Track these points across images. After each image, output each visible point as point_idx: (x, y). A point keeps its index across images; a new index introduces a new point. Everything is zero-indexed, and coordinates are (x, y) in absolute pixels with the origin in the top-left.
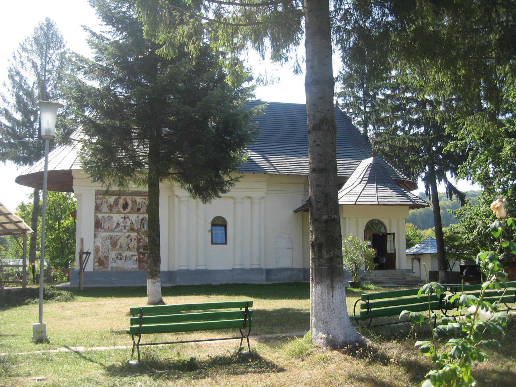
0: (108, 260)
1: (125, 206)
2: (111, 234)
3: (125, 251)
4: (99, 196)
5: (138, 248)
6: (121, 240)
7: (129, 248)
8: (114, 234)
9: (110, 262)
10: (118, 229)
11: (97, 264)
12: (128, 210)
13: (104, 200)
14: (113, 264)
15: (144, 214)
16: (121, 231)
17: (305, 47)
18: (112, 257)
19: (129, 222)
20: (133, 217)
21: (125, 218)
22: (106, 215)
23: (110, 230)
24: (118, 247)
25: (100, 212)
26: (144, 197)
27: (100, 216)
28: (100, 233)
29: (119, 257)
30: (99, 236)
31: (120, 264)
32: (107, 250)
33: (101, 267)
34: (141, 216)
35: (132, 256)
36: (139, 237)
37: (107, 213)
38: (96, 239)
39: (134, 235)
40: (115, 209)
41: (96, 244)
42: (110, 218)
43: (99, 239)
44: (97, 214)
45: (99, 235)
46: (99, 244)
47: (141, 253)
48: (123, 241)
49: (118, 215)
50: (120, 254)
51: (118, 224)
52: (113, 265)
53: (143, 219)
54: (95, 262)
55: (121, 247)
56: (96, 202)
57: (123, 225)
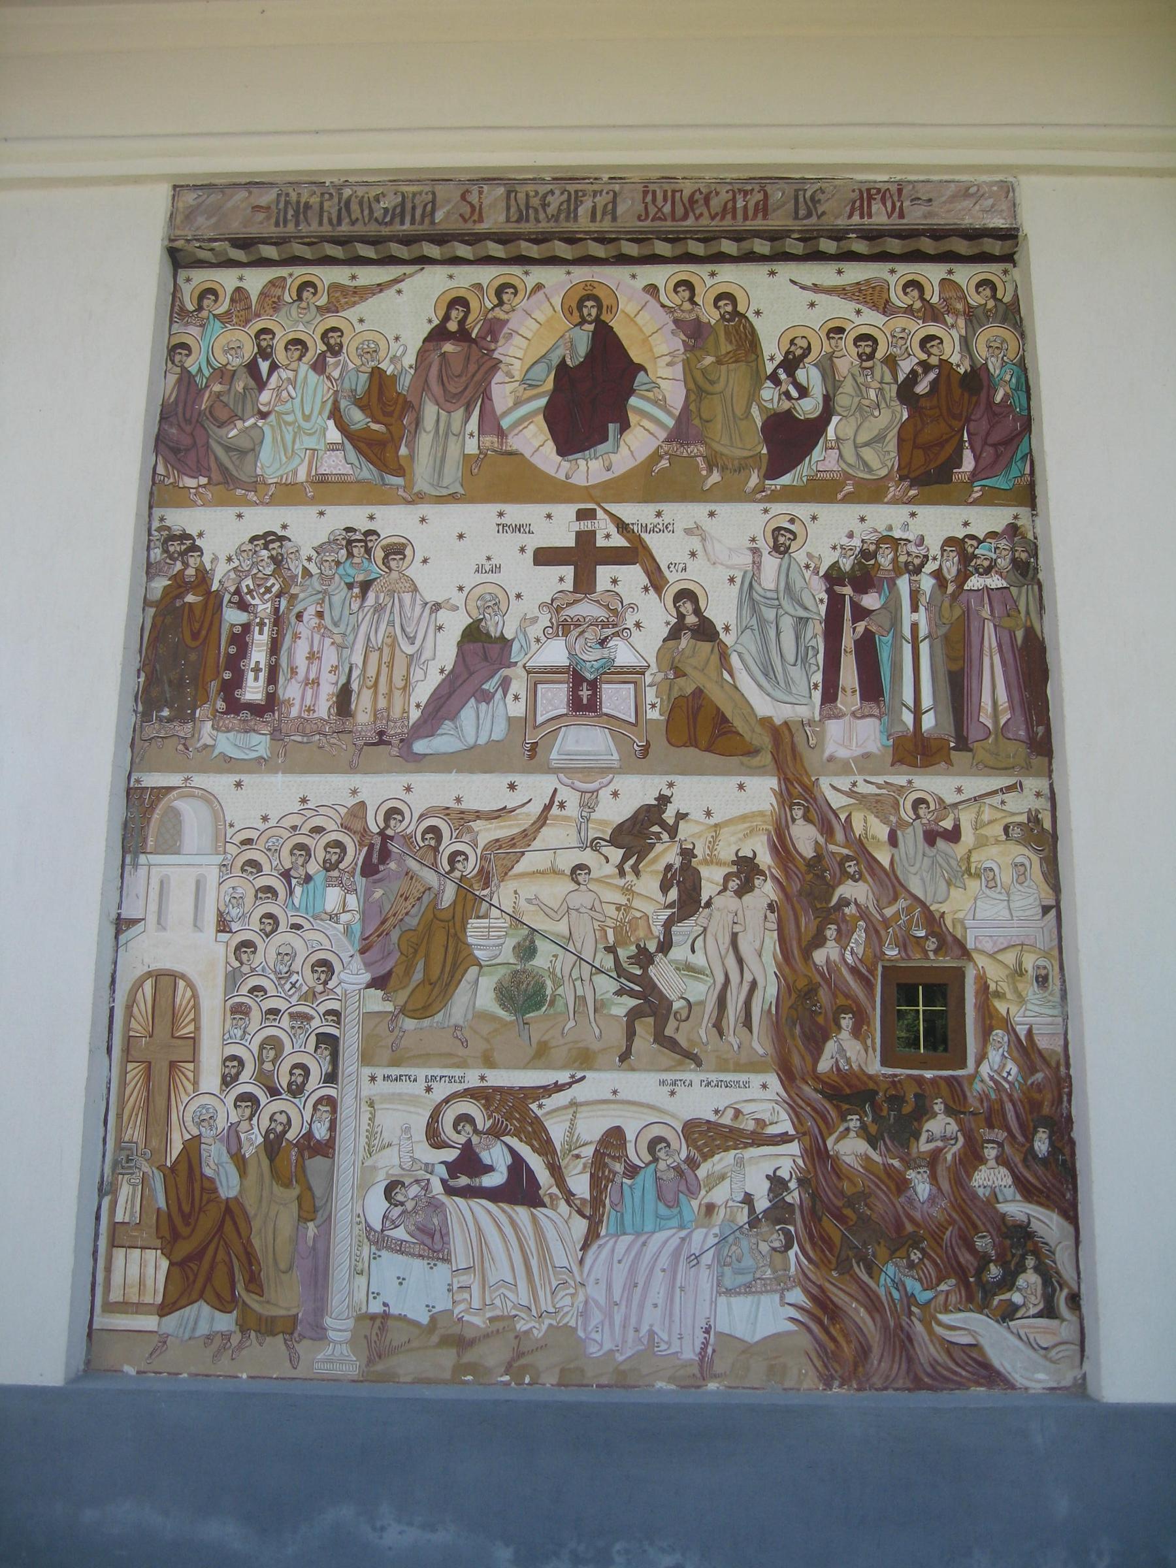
0: (311, 1207)
1: (592, 394)
2: (378, 789)
3: (585, 1059)
4: (227, 280)
5: (805, 1016)
6: (530, 893)
7: (652, 1005)
8: (428, 791)
9: (344, 1242)
10: (477, 724)
11: (145, 1270)
12: (637, 443)
13: (285, 325)
14: (390, 1265)
15: (871, 492)
16: (528, 749)
17: (455, 650)
18: (389, 1163)
19: (654, 617)
20: (715, 544)
21: (584, 557)
22: (309, 528)
23: (357, 733)
24: (478, 994)
25: (233, 483)
26: (855, 273)
27: (221, 533)
28: (219, 783)
29: (498, 1159)
30: (193, 818)
31: (506, 1275)
32: (300, 1050)
33: (206, 1318)
34: (832, 532)
35: (709, 1137)
36: (805, 837)
37: (324, 490)
38: (157, 866)
39: (726, 806)
40: (442, 440)
41: (148, 951)
42: (370, 561)
43: (187, 882)
44: (180, 519)
45: (192, 815)
46: (180, 943)
47: (848, 1093)
48: (556, 900)
49: (479, 517)
50: (514, 1111)
51: (483, 650)
52: (399, 1280)
53: (857, 576)
54: (108, 1237)
55: (524, 995)
56: (177, 349)
57: (555, 653)
